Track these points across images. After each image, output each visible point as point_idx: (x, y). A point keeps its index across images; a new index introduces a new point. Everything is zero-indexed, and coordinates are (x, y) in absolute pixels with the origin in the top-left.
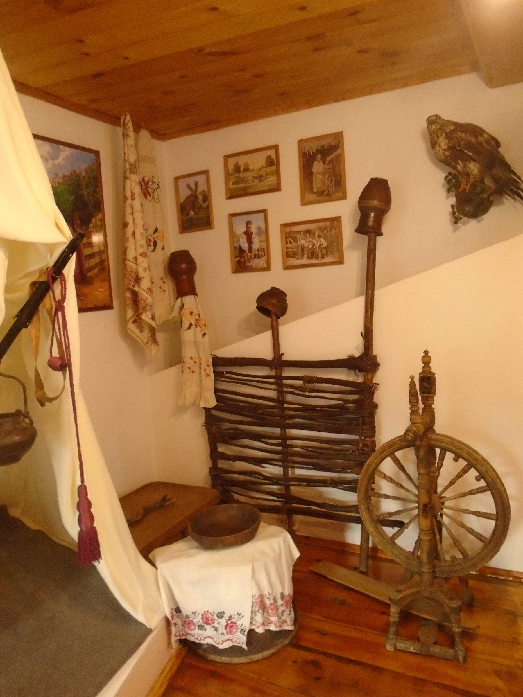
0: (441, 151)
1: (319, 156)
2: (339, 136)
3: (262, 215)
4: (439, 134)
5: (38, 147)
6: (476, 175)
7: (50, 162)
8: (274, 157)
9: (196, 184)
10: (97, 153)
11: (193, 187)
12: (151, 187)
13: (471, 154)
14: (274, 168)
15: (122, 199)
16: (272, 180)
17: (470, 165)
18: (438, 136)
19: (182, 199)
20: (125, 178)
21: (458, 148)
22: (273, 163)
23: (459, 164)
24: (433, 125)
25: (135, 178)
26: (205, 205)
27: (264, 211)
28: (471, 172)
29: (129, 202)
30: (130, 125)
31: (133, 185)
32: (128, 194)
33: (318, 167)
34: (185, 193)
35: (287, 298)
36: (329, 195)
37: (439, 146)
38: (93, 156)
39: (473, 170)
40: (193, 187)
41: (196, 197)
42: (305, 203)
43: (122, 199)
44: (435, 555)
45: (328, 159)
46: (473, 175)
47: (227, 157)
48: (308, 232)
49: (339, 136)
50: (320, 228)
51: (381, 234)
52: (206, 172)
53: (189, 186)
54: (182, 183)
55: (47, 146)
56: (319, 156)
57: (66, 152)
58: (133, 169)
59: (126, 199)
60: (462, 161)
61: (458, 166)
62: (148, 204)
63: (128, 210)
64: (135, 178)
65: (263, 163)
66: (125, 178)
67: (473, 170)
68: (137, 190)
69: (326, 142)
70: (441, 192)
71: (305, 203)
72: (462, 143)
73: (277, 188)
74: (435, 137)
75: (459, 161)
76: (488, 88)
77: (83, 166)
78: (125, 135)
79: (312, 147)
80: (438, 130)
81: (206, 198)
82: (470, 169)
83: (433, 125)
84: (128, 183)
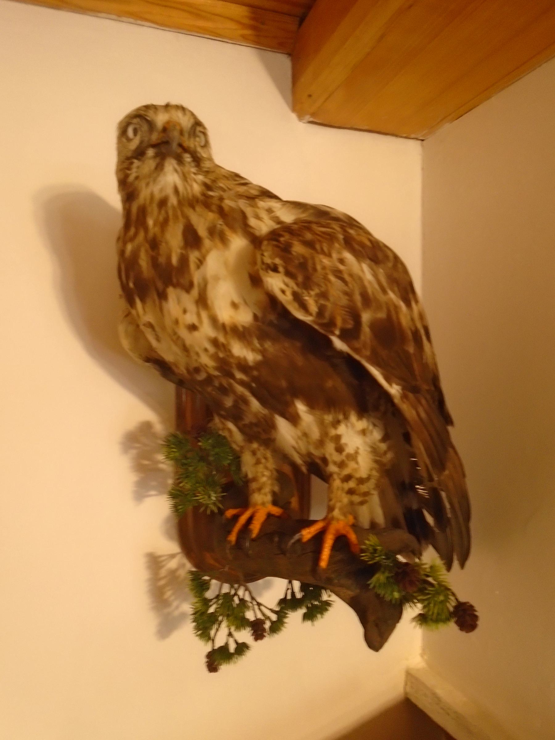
0: (207, 330)
4: (202, 232)
6: (361, 481)
13: (394, 390)
17: (342, 429)
18: (192, 239)
21: (339, 344)
23: (294, 419)
24: (170, 165)
28: (342, 465)
37: (202, 301)
39: (353, 457)
46: (347, 478)
60: (311, 405)
61: (282, 424)
67: (353, 457)
70: (117, 471)
72: (366, 317)
74: (174, 239)
75: (301, 407)
76: (294, 116)
80: (192, 202)
82: (340, 449)
83: (170, 165)
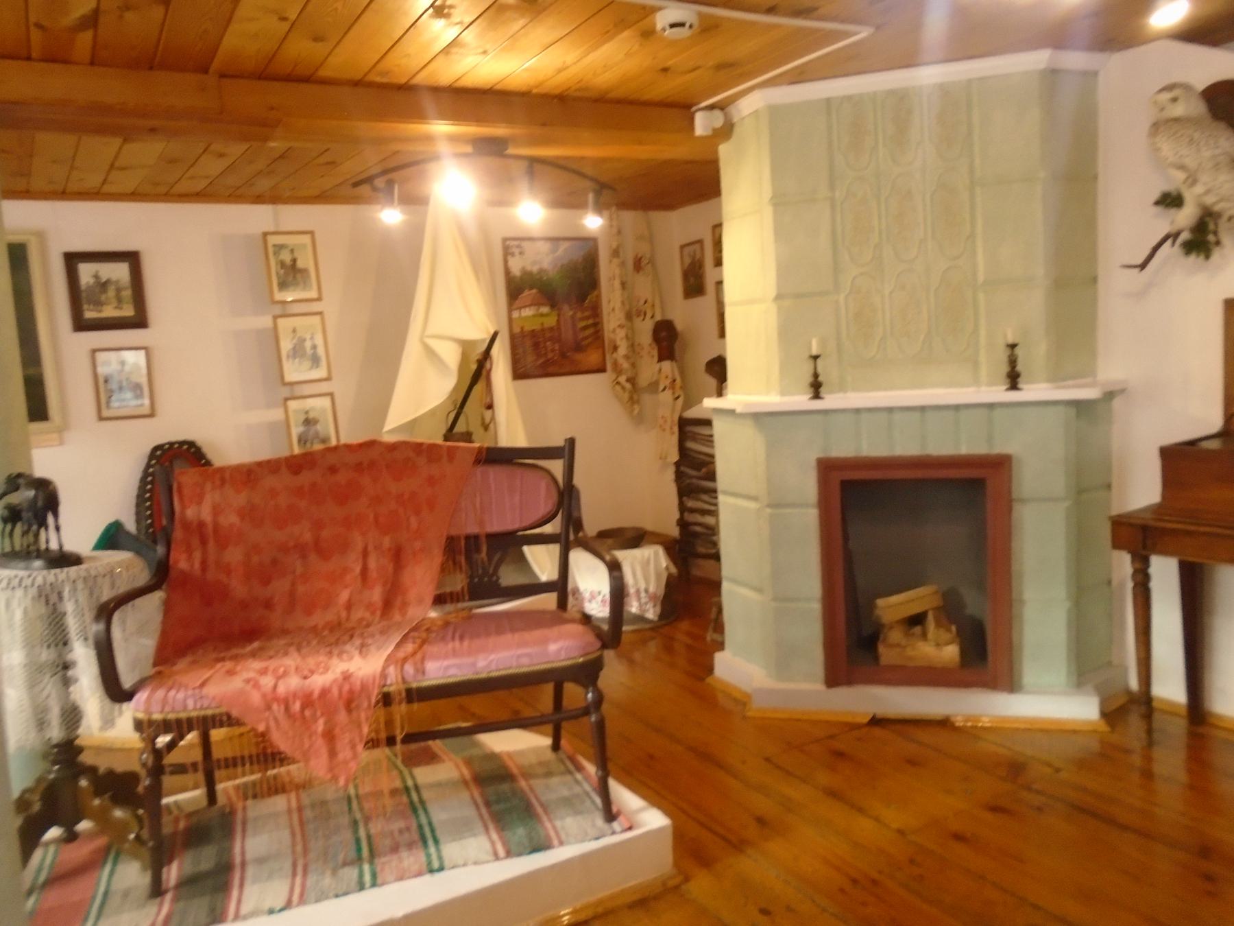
77: (578, 255)
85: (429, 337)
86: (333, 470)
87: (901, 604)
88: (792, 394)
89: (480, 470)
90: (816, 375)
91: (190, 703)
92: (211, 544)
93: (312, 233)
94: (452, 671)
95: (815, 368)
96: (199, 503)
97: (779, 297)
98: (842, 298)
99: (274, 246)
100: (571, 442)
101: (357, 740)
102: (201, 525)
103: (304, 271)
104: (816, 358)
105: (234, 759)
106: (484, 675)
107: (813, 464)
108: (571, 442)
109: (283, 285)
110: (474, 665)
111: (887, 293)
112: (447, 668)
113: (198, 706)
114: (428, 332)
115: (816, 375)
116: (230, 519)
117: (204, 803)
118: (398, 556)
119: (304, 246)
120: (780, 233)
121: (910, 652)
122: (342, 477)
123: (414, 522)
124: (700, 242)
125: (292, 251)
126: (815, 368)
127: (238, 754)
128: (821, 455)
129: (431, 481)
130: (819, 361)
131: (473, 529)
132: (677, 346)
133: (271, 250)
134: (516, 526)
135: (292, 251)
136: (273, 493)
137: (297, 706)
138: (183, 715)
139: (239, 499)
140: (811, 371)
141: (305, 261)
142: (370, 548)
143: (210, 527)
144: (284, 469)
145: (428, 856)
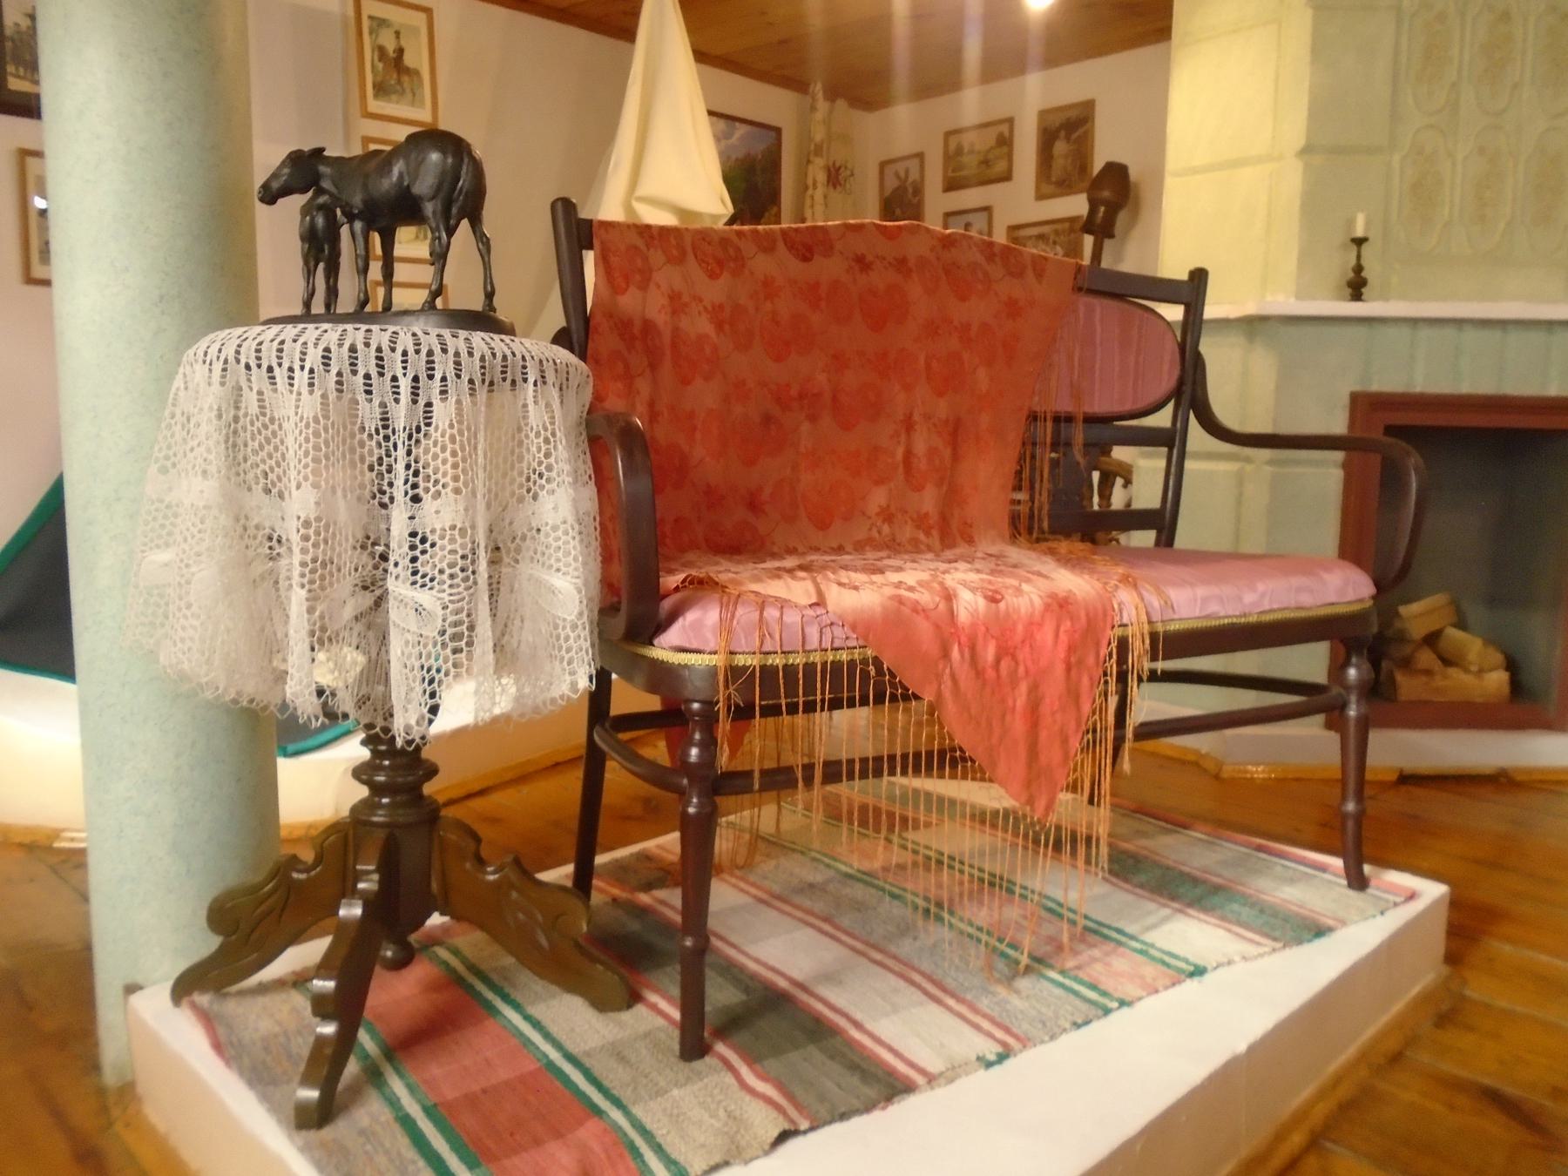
1: (1063, 134)
2: (1089, 106)
3: (985, 214)
5: (712, 125)
7: (723, 143)
8: (1007, 134)
9: (907, 172)
10: (778, 131)
11: (902, 174)
12: (844, 174)
14: (1005, 149)
15: (803, 188)
16: (1000, 167)
19: (888, 193)
20: (809, 162)
22: (1005, 142)
25: (819, 162)
26: (915, 201)
27: (987, 209)
29: (810, 192)
30: (820, 95)
31: (817, 173)
32: (810, 182)
33: (1060, 147)
34: (891, 184)
35: (306, 149)
36: (1070, 186)
38: (773, 134)
40: (902, 174)
41: (905, 189)
42: (1040, 197)
43: (803, 188)
44: (1131, 861)
45: (1075, 136)
47: (948, 134)
48: (1041, 237)
49: (1089, 106)
50: (1057, 232)
51: (1112, 236)
52: (920, 156)
53: (897, 175)
54: (889, 171)
55: (722, 124)
56: (1063, 134)
57: (741, 130)
58: (818, 151)
59: (807, 188)
62: (835, 195)
63: (808, 202)
64: (819, 162)
65: (992, 142)
66: (809, 162)
68: (821, 177)
69: (1073, 114)
71: (1040, 197)
73: (1007, 177)
77: (759, 148)
78: (813, 108)
79: (1056, 121)
81: (918, 190)
84: (810, 167)
85: (640, 199)
86: (862, 263)
87: (1421, 615)
88: (1314, 298)
89: (1084, 300)
90: (1359, 269)
91: (813, 633)
92: (667, 367)
93: (428, 11)
94: (1214, 608)
95: (1359, 257)
96: (644, 286)
97: (1306, 151)
98: (1397, 158)
99: (370, 17)
100: (1199, 277)
101: (1073, 725)
102: (648, 327)
103: (414, 73)
104: (1359, 242)
105: (878, 760)
106: (1253, 619)
107: (1345, 400)
108: (1199, 277)
109: (381, 90)
110: (1240, 599)
111: (1460, 157)
112: (1205, 600)
113: (827, 644)
114: (640, 192)
115: (1359, 269)
116: (699, 325)
117: (1506, 689)
118: (955, 432)
119: (415, 31)
120: (1318, 49)
121: (1438, 682)
122: (880, 278)
123: (982, 377)
124: (920, 156)
125: (397, 34)
126: (1359, 257)
127: (870, 754)
128: (1357, 388)
129: (1013, 309)
130: (1365, 247)
131: (1064, 405)
132: (1122, 218)
133: (366, 24)
134: (1116, 408)
135: (397, 34)
136: (768, 288)
137: (990, 653)
138: (798, 660)
139: (715, 291)
140: (1353, 262)
141: (416, 57)
142: (916, 417)
143: (667, 338)
144: (781, 246)
145: (394, 1103)
